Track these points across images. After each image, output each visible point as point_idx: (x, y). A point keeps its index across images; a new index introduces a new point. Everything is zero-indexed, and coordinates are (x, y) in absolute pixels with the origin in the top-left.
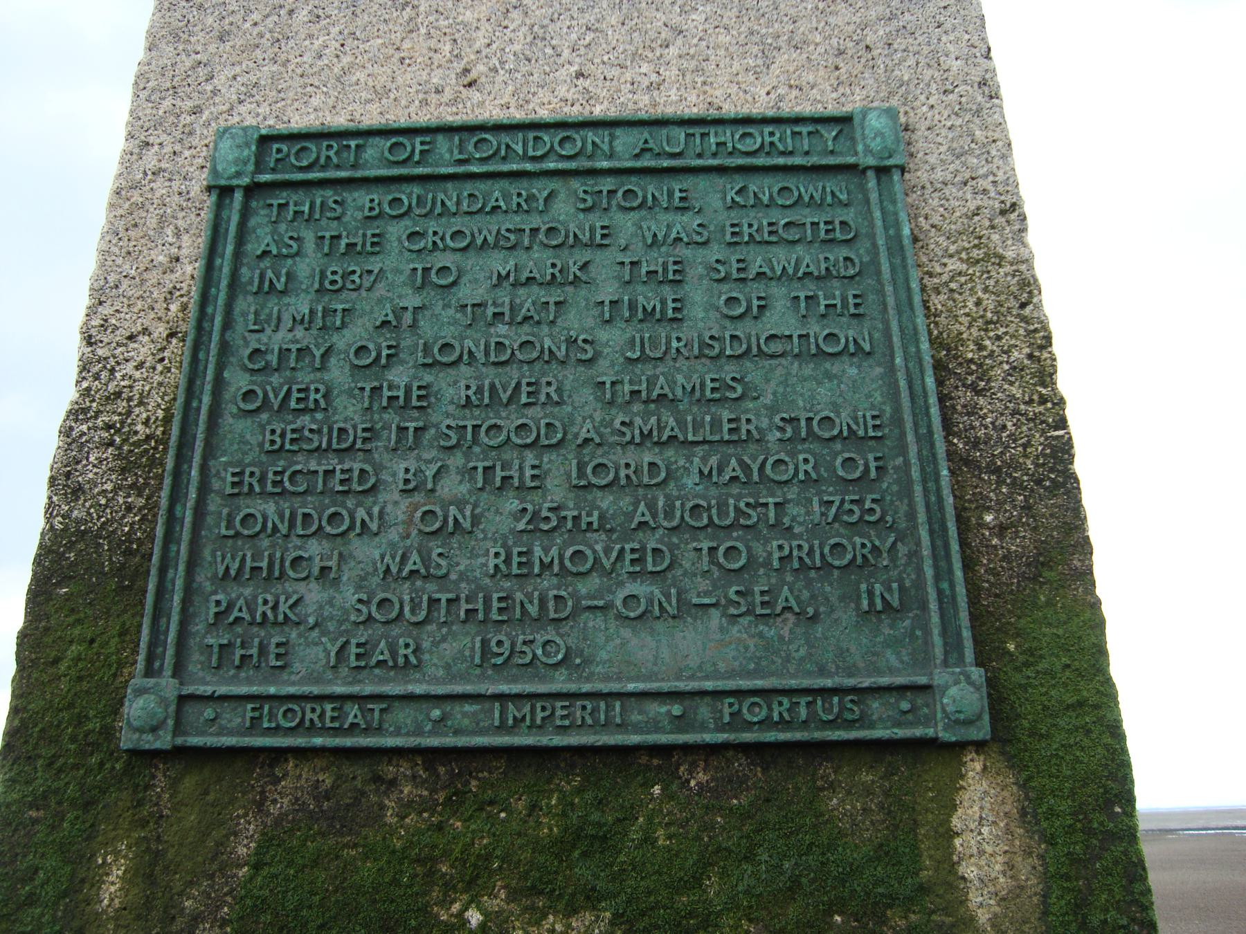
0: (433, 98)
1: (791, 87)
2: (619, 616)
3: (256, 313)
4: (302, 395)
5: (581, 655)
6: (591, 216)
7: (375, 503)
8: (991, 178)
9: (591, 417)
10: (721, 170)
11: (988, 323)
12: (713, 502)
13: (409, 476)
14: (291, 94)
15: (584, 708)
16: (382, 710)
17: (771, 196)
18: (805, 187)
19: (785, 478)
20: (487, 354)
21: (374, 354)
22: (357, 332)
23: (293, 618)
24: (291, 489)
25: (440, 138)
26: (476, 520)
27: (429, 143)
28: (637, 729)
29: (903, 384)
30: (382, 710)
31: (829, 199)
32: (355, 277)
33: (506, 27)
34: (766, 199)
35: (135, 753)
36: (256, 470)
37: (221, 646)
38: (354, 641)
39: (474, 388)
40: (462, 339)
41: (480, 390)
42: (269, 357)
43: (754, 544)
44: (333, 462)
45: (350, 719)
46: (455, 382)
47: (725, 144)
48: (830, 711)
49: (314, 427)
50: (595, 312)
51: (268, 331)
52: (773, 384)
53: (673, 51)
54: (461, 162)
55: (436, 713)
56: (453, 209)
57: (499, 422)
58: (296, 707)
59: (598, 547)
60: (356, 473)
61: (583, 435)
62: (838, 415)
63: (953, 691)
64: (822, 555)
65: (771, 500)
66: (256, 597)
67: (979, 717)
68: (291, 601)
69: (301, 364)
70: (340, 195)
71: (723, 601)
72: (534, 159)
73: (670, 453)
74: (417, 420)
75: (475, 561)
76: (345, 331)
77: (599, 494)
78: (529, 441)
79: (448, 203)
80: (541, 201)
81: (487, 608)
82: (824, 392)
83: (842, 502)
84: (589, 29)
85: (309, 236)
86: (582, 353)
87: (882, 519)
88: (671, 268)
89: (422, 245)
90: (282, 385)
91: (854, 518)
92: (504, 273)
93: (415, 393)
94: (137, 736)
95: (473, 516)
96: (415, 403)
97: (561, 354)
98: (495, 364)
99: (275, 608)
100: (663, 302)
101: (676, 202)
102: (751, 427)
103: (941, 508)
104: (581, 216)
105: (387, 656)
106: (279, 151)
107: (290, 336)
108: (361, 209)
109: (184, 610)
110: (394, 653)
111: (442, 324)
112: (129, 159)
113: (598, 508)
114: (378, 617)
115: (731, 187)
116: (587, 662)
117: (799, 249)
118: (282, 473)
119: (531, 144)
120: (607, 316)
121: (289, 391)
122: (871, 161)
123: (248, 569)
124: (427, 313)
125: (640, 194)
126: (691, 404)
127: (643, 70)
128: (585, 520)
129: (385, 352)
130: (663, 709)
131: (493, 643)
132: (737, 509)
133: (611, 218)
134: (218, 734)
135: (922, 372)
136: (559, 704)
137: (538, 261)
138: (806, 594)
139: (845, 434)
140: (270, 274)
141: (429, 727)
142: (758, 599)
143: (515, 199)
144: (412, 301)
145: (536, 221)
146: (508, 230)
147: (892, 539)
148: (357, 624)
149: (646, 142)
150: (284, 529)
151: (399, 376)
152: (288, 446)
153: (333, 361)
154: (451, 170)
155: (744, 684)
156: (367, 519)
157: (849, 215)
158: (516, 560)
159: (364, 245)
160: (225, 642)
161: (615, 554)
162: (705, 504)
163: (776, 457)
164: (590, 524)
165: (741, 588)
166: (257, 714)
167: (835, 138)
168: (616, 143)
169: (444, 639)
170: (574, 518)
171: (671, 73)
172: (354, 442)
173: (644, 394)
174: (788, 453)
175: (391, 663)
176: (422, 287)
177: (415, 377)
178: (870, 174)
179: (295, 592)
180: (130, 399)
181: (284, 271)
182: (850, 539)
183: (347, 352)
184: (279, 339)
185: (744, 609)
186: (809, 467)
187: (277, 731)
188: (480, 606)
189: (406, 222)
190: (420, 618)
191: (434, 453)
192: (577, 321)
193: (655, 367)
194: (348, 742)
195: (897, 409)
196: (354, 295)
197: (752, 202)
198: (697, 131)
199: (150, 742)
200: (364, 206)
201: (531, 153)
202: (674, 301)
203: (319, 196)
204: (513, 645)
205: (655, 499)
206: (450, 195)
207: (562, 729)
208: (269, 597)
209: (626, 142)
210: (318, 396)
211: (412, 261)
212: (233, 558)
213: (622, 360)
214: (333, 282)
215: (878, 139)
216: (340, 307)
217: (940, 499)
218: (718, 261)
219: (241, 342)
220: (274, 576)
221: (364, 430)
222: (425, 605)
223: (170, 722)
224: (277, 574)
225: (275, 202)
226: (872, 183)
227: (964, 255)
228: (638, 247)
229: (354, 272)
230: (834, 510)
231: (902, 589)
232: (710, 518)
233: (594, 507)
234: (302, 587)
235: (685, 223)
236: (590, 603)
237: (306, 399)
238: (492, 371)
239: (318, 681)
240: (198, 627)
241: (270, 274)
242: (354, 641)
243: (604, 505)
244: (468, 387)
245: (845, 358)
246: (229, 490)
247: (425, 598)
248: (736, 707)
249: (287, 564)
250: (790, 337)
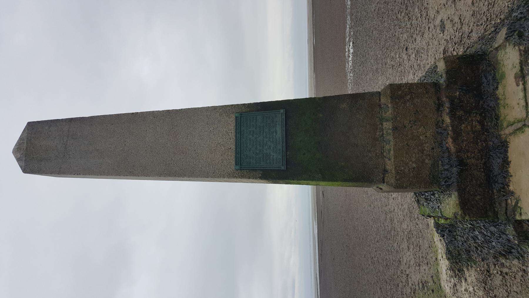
151: (258, 152)
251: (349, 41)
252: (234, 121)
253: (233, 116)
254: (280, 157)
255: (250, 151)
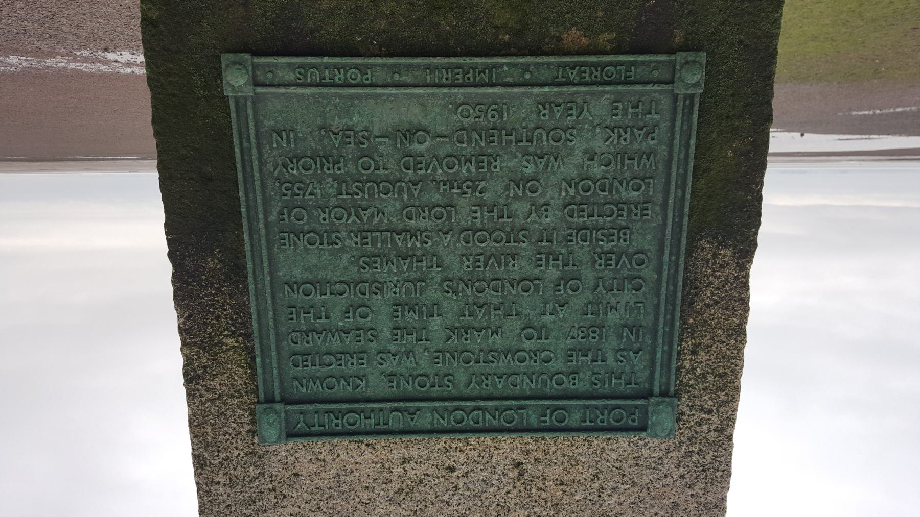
0: (540, 455)
1: (324, 460)
2: (428, 132)
3: (639, 313)
4: (609, 262)
5: (449, 110)
6: (445, 371)
7: (565, 198)
8: (203, 399)
9: (445, 247)
10: (368, 400)
11: (213, 305)
12: (376, 196)
13: (545, 213)
14: (631, 462)
15: (447, 79)
16: (557, 77)
17: (339, 384)
18: (318, 389)
19: (336, 209)
20: (503, 286)
21: (568, 286)
22: (579, 301)
23: (608, 131)
24: (612, 206)
25: (535, 425)
26: (507, 188)
27: (542, 421)
28: (418, 66)
29: (266, 264)
30: (557, 77)
31: (304, 381)
32: (581, 335)
33: (498, 505)
34: (343, 382)
35: (699, 49)
36: (634, 218)
37: (650, 113)
38: (574, 117)
39: (510, 265)
40: (518, 294)
41: (506, 265)
42: (630, 286)
43: (354, 172)
44: (590, 222)
45: (575, 72)
46: (521, 269)
47: (366, 418)
48: (312, 73)
49: (601, 243)
50: (442, 311)
51: (632, 303)
52: (342, 266)
53: (396, 486)
54: (522, 408)
55: (527, 76)
56: (525, 377)
57: (496, 244)
58: (605, 78)
59: (440, 171)
60: (575, 215)
61: (448, 236)
62: (305, 246)
63: (242, 82)
64: (316, 165)
65: (345, 197)
66: (631, 143)
67: (227, 66)
68: (611, 140)
69: (610, 282)
70: (595, 389)
71: (372, 139)
72: (479, 409)
73: (401, 226)
74: (542, 247)
75: (508, 163)
76: (586, 301)
77: (440, 202)
78: (479, 233)
79: (528, 381)
80: (474, 381)
81: (500, 136)
82: (313, 260)
83: (304, 195)
84: (447, 503)
85: (610, 361)
86: (450, 285)
87: (281, 185)
88: (399, 337)
89: (543, 355)
90: (621, 269)
91: (297, 185)
92: (495, 335)
93: (543, 263)
94: (697, 59)
95: (509, 190)
96: (543, 256)
97: (461, 285)
98: (499, 280)
99: (620, 136)
100: (403, 316)
101: (395, 379)
102: (355, 239)
103: (246, 190)
104: (451, 371)
105: (555, 109)
106: (633, 421)
107: (618, 299)
108: (580, 380)
109: (673, 134)
110: (551, 110)
111: (528, 304)
112: (730, 421)
113: (440, 194)
114: (560, 132)
115: (363, 389)
116: (445, 106)
117: (324, 350)
118: (619, 216)
119: (481, 419)
120: (436, 307)
121: (617, 265)
122: (278, 407)
123: (636, 159)
124: (538, 311)
125: (416, 385)
126: (389, 254)
127: (414, 472)
128: (447, 187)
129: (562, 287)
130: (404, 78)
131: (497, 116)
132: (363, 192)
133: (433, 369)
134: (650, 62)
135: (254, 272)
136: (460, 81)
137: (476, 342)
138: (326, 142)
139: (301, 235)
140: (633, 338)
141: (532, 68)
142: (352, 140)
143: (489, 382)
144: (548, 318)
145: (477, 368)
146: (493, 362)
147: (276, 172)
148: (573, 128)
149: (412, 419)
150: (616, 183)
151: (553, 273)
152: (616, 231)
153: (592, 284)
154: (528, 402)
155: (359, 91)
156: (568, 188)
157: (293, 371)
158: (485, 165)
159: (577, 356)
160: (648, 116)
161: (431, 167)
162: (382, 195)
163: (341, 222)
164: (445, 185)
165: (361, 146)
166: (628, 74)
167: (298, 423)
168: (430, 419)
169: (524, 119)
170: (453, 188)
171: (398, 470)
172: (577, 234)
173: (415, 260)
174: (335, 224)
175: (553, 105)
176: (542, 328)
177: (544, 272)
178: (278, 398)
179: (608, 146)
180: (714, 264)
181: (624, 340)
182: (301, 173)
183: (584, 288)
184: (628, 296)
185: (360, 134)
186: (323, 216)
187: (616, 64)
188: (504, 137)
189: (553, 370)
190: (537, 131)
191: (532, 227)
192: (451, 305)
193: (409, 276)
194: (576, 59)
195: (269, 249)
196: (581, 324)
197: (351, 380)
198: (382, 427)
199: (691, 56)
200: (579, 381)
201: (480, 412)
202: (397, 317)
203: (606, 389)
204: (486, 116)
205: (409, 199)
206: (527, 386)
207: (459, 66)
208: (623, 142)
209: (425, 421)
210: (599, 261)
211: (548, 345)
212: (645, 165)
213: (428, 281)
214: (594, 332)
215: (272, 421)
216: (589, 316)
217: (247, 195)
218: (372, 341)
219: (648, 296)
220: (623, 155)
221: (572, 241)
222: (535, 139)
223: (678, 67)
224: (619, 156)
225: (633, 386)
226: (277, 392)
227: (225, 347)
228: (418, 349)
229: (582, 338)
230: (309, 190)
231: (271, 144)
232: (378, 187)
233: (443, 195)
234: (604, 149)
235: (390, 365)
236: (444, 140)
237: (607, 260)
238: (500, 275)
239: (592, 94)
240: (665, 125)
241: (633, 338)
242: (574, 117)
243: (437, 196)
244: (514, 266)
245: (300, 281)
246: (649, 205)
247: (535, 143)
248: (364, 78)
249: (613, 162)
250: (331, 294)
251: (106, 62)
252: (320, 446)
253: (284, 453)
254: (600, 105)
255: (542, 332)
